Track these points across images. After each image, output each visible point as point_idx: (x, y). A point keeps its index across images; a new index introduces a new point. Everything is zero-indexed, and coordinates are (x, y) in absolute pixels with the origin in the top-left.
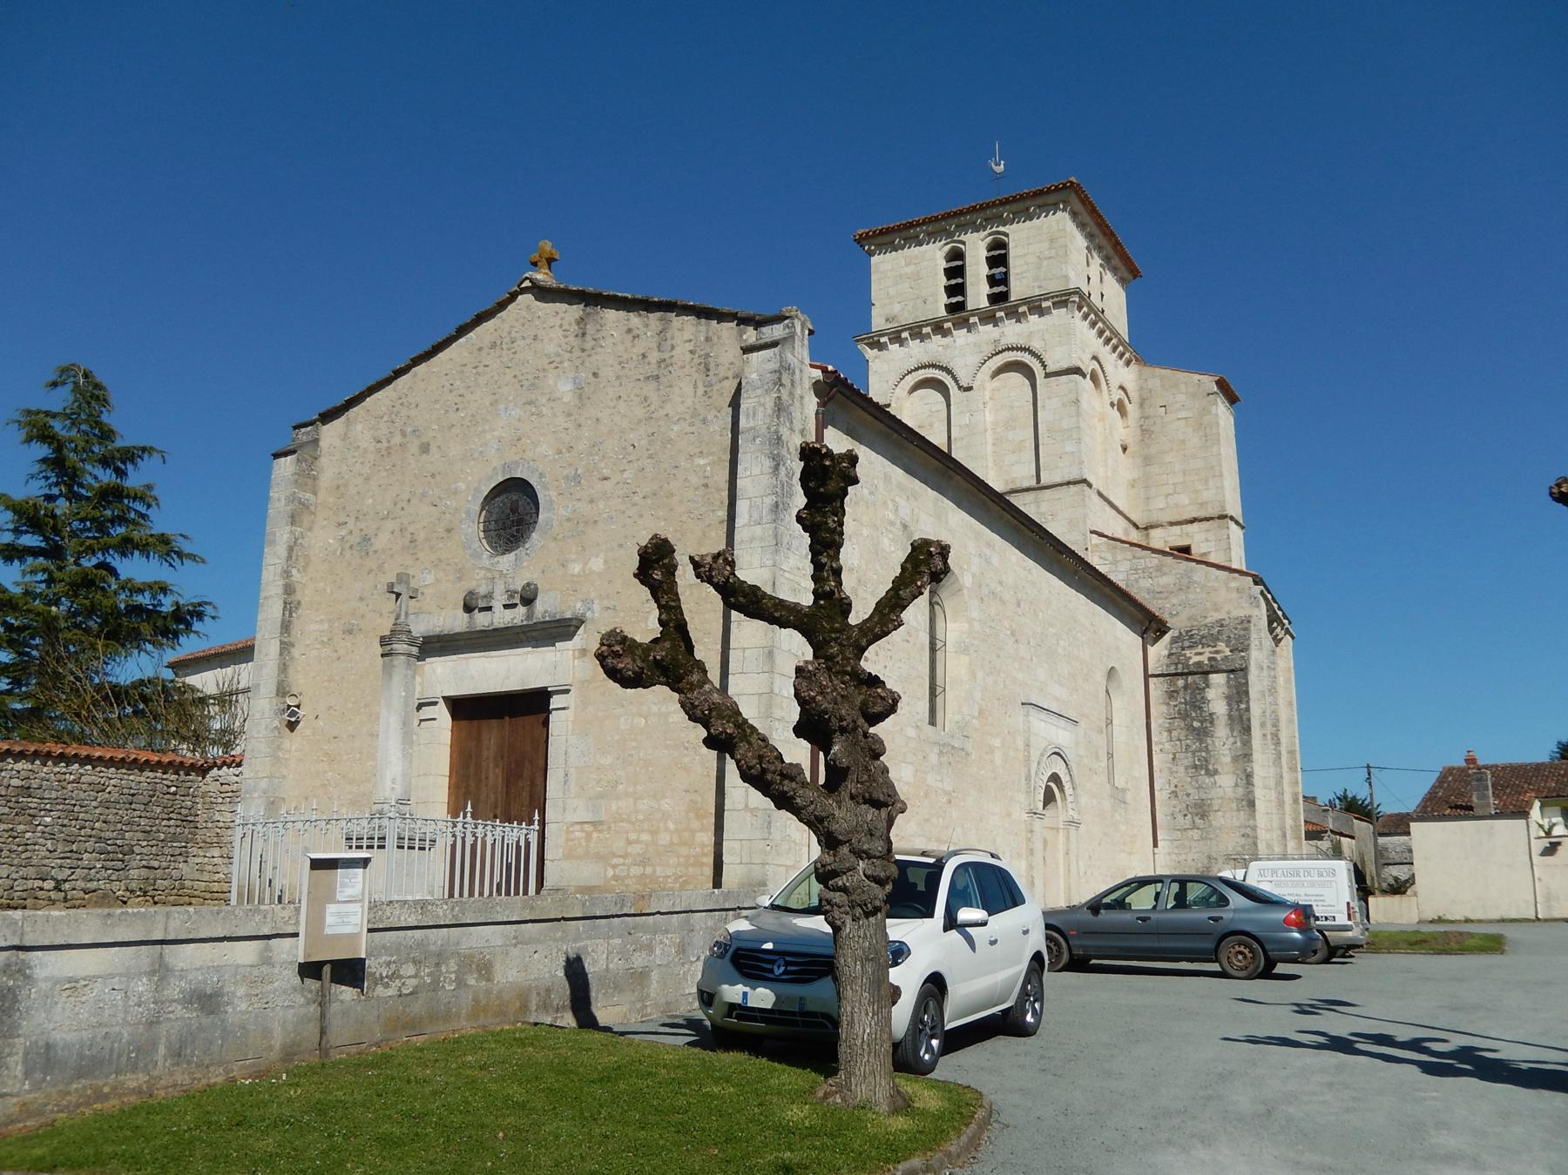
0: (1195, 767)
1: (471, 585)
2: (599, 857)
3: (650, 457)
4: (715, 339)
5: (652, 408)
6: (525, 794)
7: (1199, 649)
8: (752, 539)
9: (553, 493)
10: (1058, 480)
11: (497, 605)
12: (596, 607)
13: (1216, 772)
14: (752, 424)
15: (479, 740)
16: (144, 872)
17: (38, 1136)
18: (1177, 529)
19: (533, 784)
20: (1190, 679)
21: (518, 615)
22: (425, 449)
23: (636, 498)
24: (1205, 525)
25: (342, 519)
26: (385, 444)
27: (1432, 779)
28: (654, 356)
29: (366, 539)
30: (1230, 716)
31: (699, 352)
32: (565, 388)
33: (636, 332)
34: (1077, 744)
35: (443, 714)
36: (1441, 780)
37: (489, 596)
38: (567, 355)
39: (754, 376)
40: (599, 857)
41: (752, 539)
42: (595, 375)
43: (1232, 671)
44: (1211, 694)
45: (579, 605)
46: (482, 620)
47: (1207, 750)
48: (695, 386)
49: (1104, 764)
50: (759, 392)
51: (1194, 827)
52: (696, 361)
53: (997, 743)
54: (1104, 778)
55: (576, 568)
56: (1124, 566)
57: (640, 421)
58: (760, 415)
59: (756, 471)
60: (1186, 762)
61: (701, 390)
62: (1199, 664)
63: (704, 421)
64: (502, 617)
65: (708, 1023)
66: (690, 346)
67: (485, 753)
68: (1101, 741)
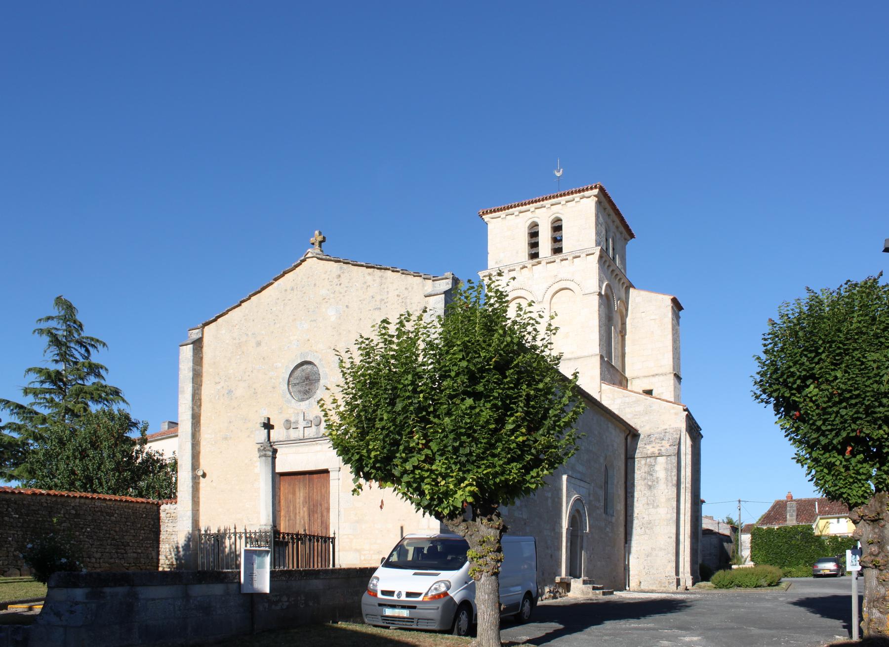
0: (648, 504)
1: (286, 417)
2: (357, 550)
4: (410, 289)
6: (319, 521)
7: (653, 445)
10: (586, 354)
13: (658, 506)
15: (294, 494)
16: (135, 555)
18: (646, 380)
19: (322, 516)
20: (648, 460)
22: (259, 344)
24: (661, 378)
27: (771, 505)
28: (378, 298)
29: (230, 392)
30: (666, 479)
31: (402, 296)
32: (332, 314)
34: (589, 495)
36: (773, 507)
37: (297, 422)
38: (332, 296)
40: (357, 550)
42: (347, 306)
44: (657, 468)
47: (654, 496)
49: (602, 504)
51: (645, 533)
52: (400, 301)
53: (549, 495)
54: (602, 511)
56: (618, 401)
60: (643, 502)
62: (653, 453)
65: (227, 550)
66: (397, 293)
67: (298, 501)
68: (601, 493)
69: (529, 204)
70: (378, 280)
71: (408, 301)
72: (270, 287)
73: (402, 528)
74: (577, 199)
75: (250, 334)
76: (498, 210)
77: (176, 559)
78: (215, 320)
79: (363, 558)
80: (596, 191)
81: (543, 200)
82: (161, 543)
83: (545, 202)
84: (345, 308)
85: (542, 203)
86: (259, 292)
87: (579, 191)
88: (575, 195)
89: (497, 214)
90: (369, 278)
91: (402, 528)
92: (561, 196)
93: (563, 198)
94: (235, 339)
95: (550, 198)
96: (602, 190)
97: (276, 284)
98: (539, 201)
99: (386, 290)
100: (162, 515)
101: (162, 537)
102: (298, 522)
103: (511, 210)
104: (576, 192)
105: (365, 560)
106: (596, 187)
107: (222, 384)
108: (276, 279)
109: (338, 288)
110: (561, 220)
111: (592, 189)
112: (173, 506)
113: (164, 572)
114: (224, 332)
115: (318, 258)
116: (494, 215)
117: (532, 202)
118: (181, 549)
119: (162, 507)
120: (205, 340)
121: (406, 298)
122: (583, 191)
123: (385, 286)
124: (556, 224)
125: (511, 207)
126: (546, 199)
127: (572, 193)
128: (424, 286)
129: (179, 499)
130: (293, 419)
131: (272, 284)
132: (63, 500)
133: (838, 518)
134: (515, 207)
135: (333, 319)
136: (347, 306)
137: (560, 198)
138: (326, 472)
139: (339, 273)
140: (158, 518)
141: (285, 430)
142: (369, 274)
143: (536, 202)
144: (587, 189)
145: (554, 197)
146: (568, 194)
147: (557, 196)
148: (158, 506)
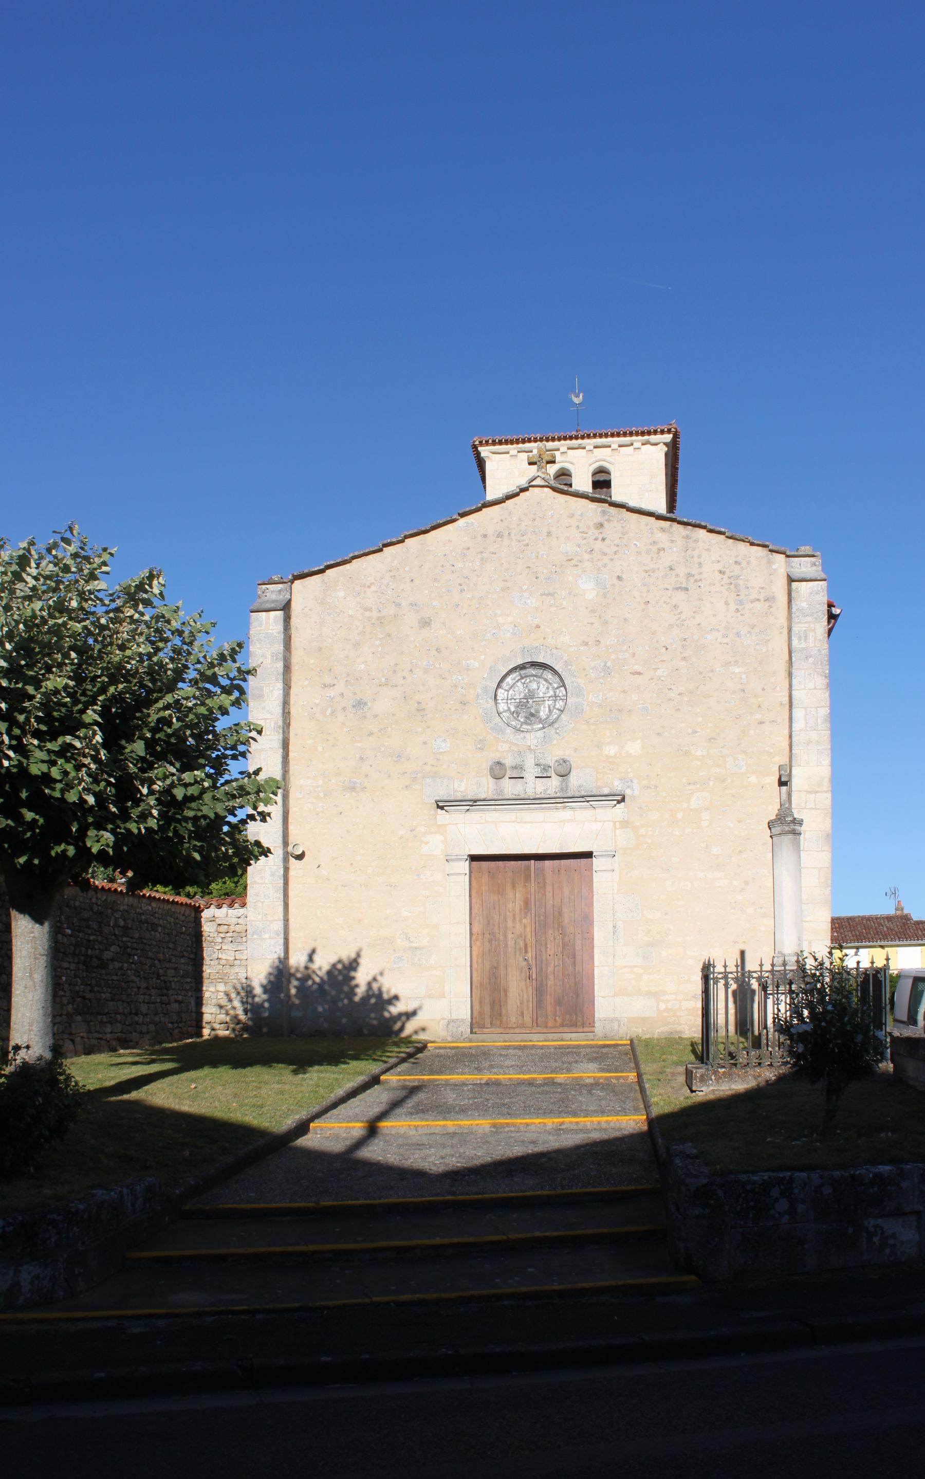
1: (497, 756)
2: (649, 994)
3: (684, 658)
4: (744, 564)
5: (683, 617)
8: (809, 742)
9: (581, 681)
11: (531, 772)
12: (635, 785)
14: (803, 645)
17: (578, 1054)
21: (553, 785)
23: (672, 694)
25: (328, 680)
26: (375, 614)
28: (682, 570)
31: (728, 574)
32: (588, 588)
33: (660, 545)
35: (465, 866)
37: (519, 767)
38: (587, 556)
39: (804, 604)
40: (649, 994)
41: (809, 742)
42: (619, 578)
43: (643, 1090)
45: (616, 783)
46: (510, 788)
48: (727, 604)
50: (809, 619)
52: (726, 580)
55: (612, 750)
57: (671, 626)
58: (811, 640)
59: (811, 685)
61: (733, 607)
63: (738, 634)
64: (533, 786)
66: (719, 567)
69: (559, 439)
70: (680, 542)
71: (741, 582)
72: (450, 526)
73: (742, 953)
74: (636, 445)
75: (404, 603)
76: (507, 442)
77: (246, 1011)
78: (322, 571)
79: (662, 1006)
80: (668, 437)
81: (583, 438)
82: (206, 983)
83: (586, 441)
84: (616, 582)
85: (580, 441)
86: (426, 532)
87: (643, 434)
88: (634, 438)
89: (504, 448)
90: (662, 537)
91: (742, 953)
92: (612, 435)
93: (616, 439)
94: (366, 609)
95: (595, 436)
96: (676, 436)
97: (462, 522)
98: (576, 438)
99: (696, 560)
100: (207, 928)
101: (208, 970)
102: (511, 943)
103: (527, 445)
104: (637, 434)
105: (666, 1010)
106: (669, 431)
107: (340, 687)
108: (463, 515)
109: (598, 545)
110: (608, 473)
111: (662, 432)
112: (237, 911)
113: (216, 1040)
114: (341, 594)
115: (554, 489)
116: (498, 448)
117: (565, 439)
118: (258, 990)
119: (206, 914)
120: (293, 604)
121: (738, 577)
122: (649, 433)
123: (696, 553)
124: (602, 477)
125: (529, 441)
126: (589, 437)
127: (631, 434)
128: (770, 562)
129: (250, 899)
130: (509, 761)
131: (454, 521)
132: (111, 898)
133: (858, 948)
134: (535, 441)
135: (590, 595)
136: (619, 578)
137: (610, 439)
138: (588, 855)
139: (599, 519)
140: (197, 936)
141: (491, 780)
142: (663, 530)
143: (571, 438)
144: (655, 432)
145: (601, 436)
146: (625, 435)
147: (606, 436)
148: (198, 910)
